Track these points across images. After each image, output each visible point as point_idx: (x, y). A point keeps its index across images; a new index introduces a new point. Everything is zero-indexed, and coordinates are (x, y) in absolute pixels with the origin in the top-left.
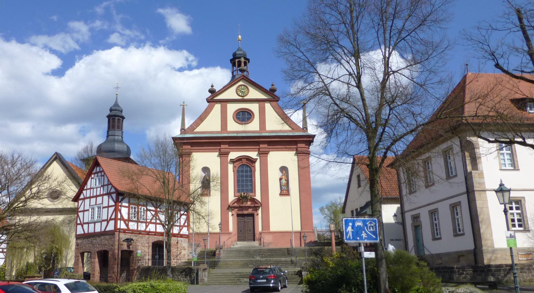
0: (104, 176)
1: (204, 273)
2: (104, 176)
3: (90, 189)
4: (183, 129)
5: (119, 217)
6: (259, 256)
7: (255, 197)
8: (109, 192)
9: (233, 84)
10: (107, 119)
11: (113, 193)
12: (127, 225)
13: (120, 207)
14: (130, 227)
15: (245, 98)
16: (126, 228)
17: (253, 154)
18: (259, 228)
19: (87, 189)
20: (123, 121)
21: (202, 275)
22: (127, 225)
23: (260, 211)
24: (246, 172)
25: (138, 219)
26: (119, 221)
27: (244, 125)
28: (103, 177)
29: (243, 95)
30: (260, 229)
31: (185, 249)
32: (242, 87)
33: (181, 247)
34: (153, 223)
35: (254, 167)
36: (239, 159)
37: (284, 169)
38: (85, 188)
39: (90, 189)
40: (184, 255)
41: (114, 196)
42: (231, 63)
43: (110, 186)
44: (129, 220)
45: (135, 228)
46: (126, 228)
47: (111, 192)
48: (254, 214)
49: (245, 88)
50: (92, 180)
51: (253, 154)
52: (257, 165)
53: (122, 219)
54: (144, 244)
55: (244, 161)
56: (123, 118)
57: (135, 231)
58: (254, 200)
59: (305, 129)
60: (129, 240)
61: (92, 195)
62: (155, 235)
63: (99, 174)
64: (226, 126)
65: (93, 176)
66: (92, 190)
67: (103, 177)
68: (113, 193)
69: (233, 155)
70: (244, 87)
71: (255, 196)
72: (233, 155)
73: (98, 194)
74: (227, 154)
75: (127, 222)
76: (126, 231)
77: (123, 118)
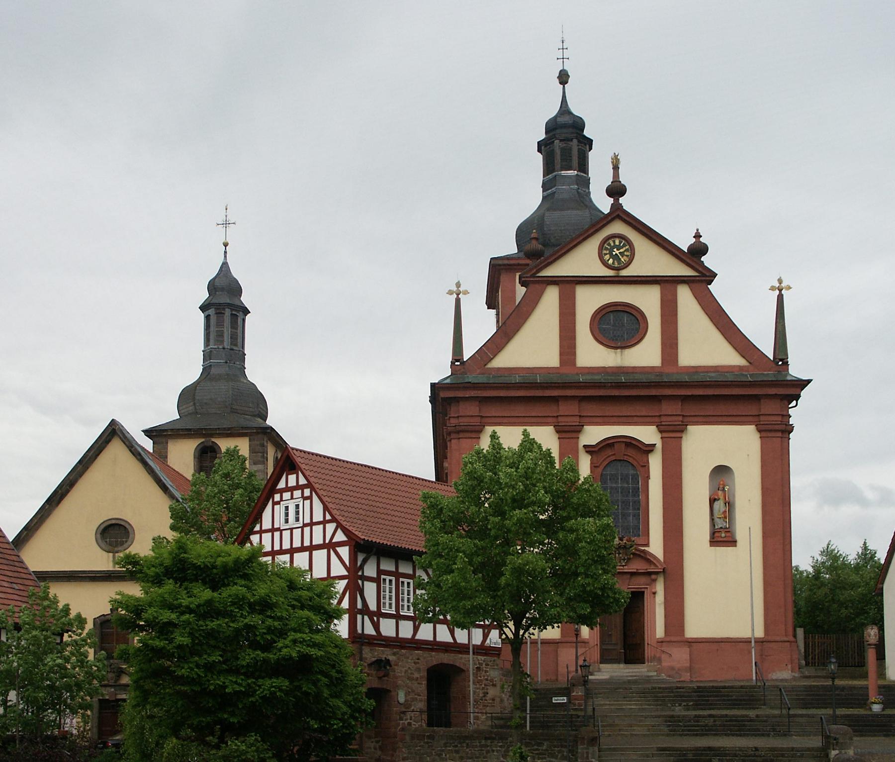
0: (310, 498)
1: (591, 750)
2: (310, 498)
3: (273, 530)
4: (457, 361)
5: (359, 606)
6: (680, 705)
7: (646, 548)
8: (327, 541)
9: (590, 232)
10: (201, 316)
11: (341, 544)
12: (376, 626)
13: (360, 582)
14: (381, 630)
15: (624, 273)
16: (374, 633)
17: (647, 434)
18: (658, 626)
19: (261, 532)
20: (244, 320)
21: (587, 753)
22: (376, 626)
23: (660, 587)
24: (625, 478)
25: (397, 609)
26: (359, 617)
27: (619, 350)
28: (307, 502)
29: (616, 265)
30: (660, 632)
31: (494, 685)
32: (614, 242)
33: (487, 680)
34: (429, 621)
35: (646, 466)
36: (608, 444)
37: (721, 472)
38: (257, 528)
39: (273, 530)
40: (493, 700)
41: (344, 552)
42: (539, 150)
43: (331, 527)
44: (379, 614)
45: (393, 634)
46: (374, 633)
47: (334, 541)
48: (644, 592)
49: (624, 246)
50: (276, 507)
51: (647, 434)
52: (655, 463)
53: (365, 611)
54: (412, 674)
55: (620, 449)
56: (246, 311)
57: (391, 642)
58: (646, 558)
59: (780, 363)
60: (381, 665)
61: (277, 547)
62: (432, 650)
63: (297, 493)
64: (574, 354)
65: (277, 497)
66: (277, 534)
67: (307, 502)
68: (341, 544)
69: (594, 434)
70: (620, 242)
71: (647, 545)
72: (594, 434)
73: (297, 544)
74: (577, 430)
75: (375, 618)
76: (376, 642)
77: (246, 311)
